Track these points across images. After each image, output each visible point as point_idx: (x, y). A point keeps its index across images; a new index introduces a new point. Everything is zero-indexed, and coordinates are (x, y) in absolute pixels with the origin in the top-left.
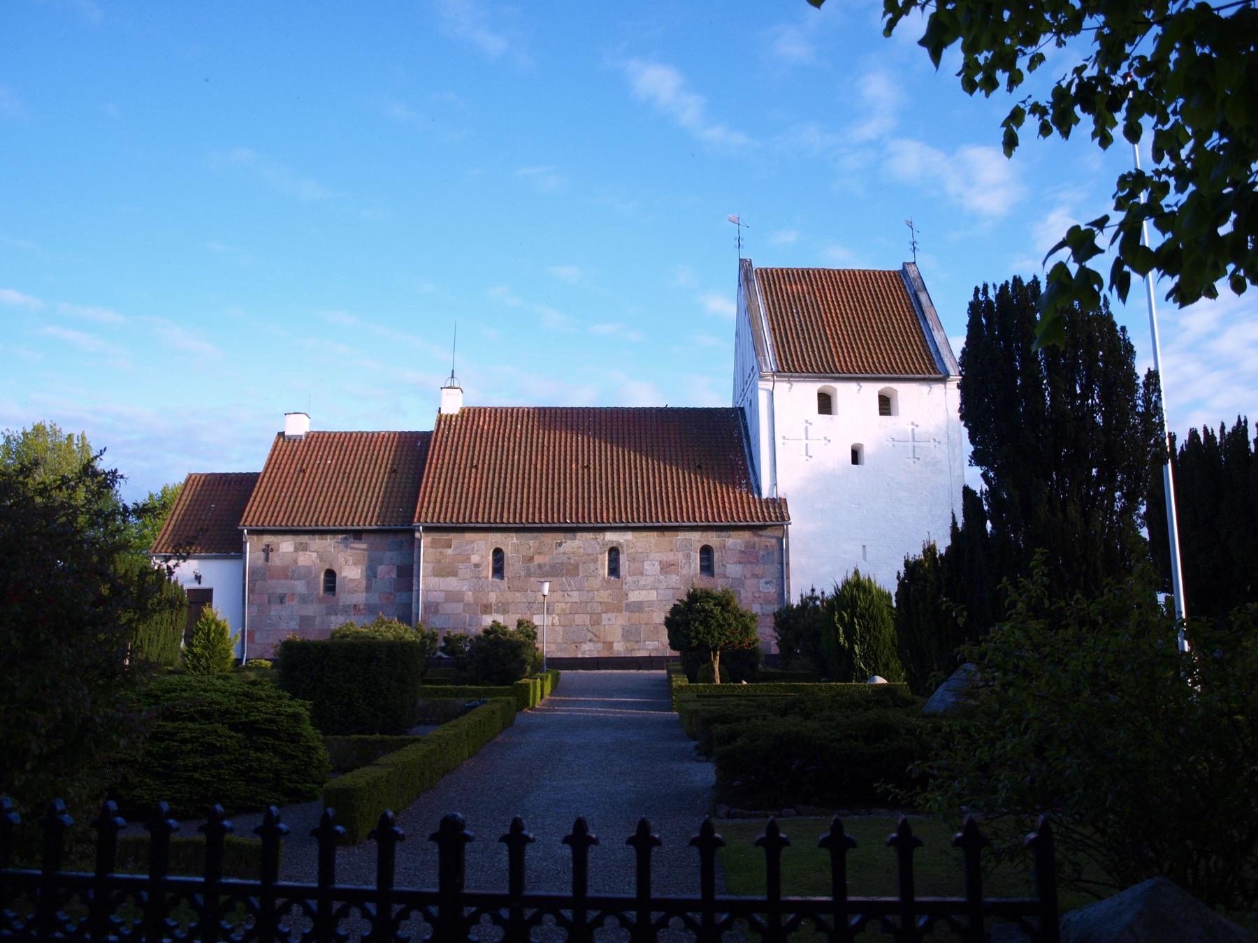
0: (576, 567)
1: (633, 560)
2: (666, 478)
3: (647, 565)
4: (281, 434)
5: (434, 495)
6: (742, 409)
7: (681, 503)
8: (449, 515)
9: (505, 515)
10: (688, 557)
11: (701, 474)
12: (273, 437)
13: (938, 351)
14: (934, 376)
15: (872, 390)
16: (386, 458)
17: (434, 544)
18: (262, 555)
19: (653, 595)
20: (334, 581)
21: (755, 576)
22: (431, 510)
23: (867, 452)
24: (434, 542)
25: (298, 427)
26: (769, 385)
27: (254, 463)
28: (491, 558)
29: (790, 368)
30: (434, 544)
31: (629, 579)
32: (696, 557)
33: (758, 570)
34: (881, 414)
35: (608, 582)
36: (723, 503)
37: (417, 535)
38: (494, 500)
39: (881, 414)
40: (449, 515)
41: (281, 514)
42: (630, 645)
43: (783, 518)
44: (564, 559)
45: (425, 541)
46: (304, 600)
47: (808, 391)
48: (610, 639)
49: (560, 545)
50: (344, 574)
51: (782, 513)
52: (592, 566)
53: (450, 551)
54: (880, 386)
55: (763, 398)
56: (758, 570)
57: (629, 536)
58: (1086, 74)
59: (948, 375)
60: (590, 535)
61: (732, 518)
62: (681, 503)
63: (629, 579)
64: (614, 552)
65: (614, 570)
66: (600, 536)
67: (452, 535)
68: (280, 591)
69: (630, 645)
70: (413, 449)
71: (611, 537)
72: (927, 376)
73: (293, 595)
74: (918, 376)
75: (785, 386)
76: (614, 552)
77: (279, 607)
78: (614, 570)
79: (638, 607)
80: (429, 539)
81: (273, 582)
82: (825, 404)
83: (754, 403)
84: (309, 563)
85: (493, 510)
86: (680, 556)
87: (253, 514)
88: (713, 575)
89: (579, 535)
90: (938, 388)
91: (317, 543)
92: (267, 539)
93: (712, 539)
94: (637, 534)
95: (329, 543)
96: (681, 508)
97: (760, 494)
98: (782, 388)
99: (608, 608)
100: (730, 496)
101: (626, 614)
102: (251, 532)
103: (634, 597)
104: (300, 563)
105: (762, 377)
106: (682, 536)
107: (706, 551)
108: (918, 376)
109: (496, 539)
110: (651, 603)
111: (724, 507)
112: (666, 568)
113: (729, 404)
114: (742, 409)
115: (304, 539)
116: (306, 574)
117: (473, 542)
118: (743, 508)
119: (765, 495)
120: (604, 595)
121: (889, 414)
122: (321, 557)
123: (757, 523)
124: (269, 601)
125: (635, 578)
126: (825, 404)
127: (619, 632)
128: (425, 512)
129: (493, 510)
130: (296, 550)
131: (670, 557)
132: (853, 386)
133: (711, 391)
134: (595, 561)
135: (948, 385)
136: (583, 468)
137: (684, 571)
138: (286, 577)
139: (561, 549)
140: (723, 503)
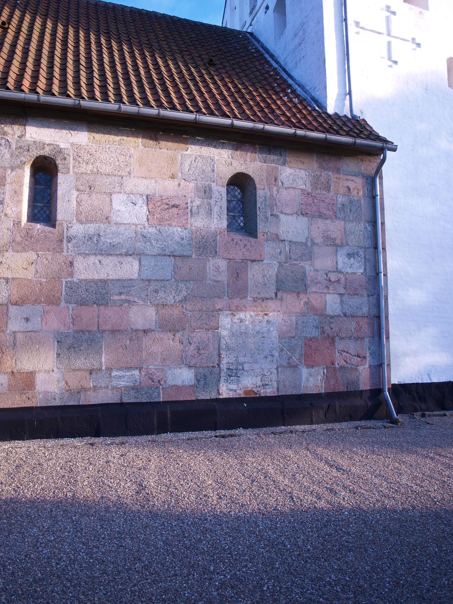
64: (45, 171)
76: (45, 171)
88: (256, 237)
110: (125, 285)
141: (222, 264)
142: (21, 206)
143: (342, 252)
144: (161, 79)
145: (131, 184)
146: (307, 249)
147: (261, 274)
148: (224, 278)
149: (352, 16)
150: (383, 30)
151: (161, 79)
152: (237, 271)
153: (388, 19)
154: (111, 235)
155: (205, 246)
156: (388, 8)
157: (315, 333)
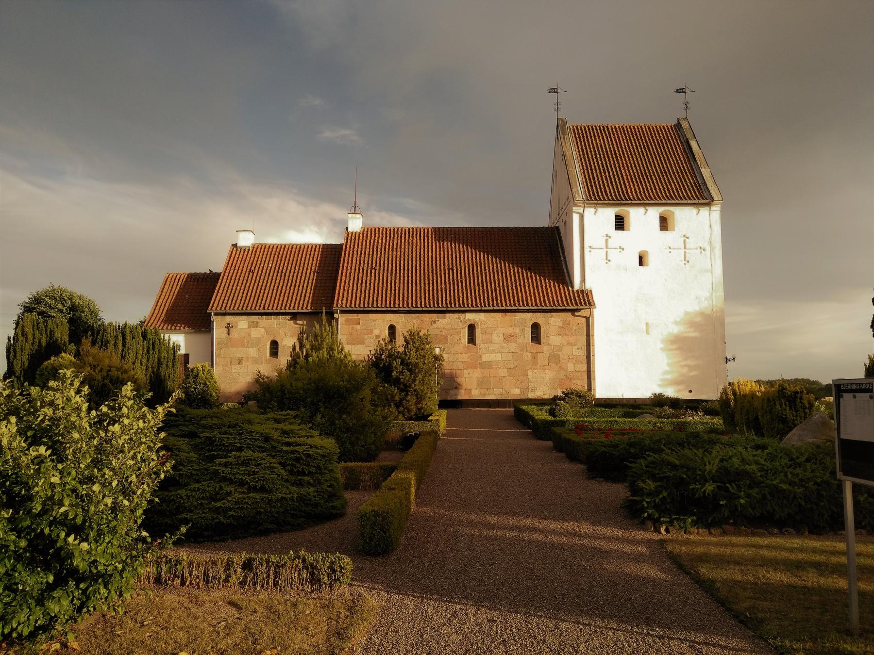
0: (446, 338)
1: (485, 333)
2: (506, 277)
3: (494, 336)
4: (235, 245)
5: (346, 288)
6: (558, 228)
7: (517, 294)
8: (358, 302)
9: (397, 302)
10: (523, 330)
11: (544, 277)
12: (228, 249)
13: (705, 183)
14: (702, 201)
15: (654, 214)
16: (314, 263)
17: (348, 322)
18: (226, 330)
19: (498, 357)
20: (277, 348)
21: (570, 344)
22: (345, 299)
23: (651, 259)
24: (347, 320)
25: (246, 240)
26: (581, 210)
27: (218, 265)
28: (387, 332)
29: (598, 195)
30: (348, 322)
31: (482, 346)
32: (528, 330)
33: (572, 339)
34: (661, 230)
35: (468, 348)
36: (547, 293)
37: (336, 316)
38: (389, 292)
39: (661, 230)
40: (358, 302)
41: (238, 302)
42: (483, 391)
43: (590, 304)
44: (438, 332)
45: (342, 318)
46: (256, 361)
47: (608, 214)
48: (469, 387)
49: (435, 322)
50: (284, 343)
51: (589, 300)
52: (457, 337)
53: (359, 327)
54: (661, 209)
55: (576, 218)
56: (572, 339)
57: (482, 316)
58: (39, 622)
59: (713, 200)
60: (456, 315)
61: (554, 304)
62: (517, 294)
63: (482, 346)
64: (472, 328)
65: (472, 339)
66: (462, 316)
67: (360, 316)
68: (238, 355)
69: (483, 391)
70: (330, 257)
71: (470, 317)
72: (697, 201)
73: (248, 358)
74: (690, 201)
75: (592, 210)
76: (472, 328)
77: (238, 367)
78: (472, 339)
79: (488, 365)
80: (344, 319)
81: (233, 350)
82: (620, 223)
83: (568, 224)
84: (259, 336)
85: (388, 299)
86: (517, 330)
87: (217, 302)
88: (540, 344)
89: (448, 315)
90: (704, 211)
91: (264, 321)
92: (228, 319)
93: (539, 318)
94: (486, 314)
95: (273, 321)
96: (518, 297)
97: (572, 287)
98: (589, 212)
99: (469, 366)
100: (551, 287)
101: (480, 370)
102: (216, 314)
103: (486, 358)
104: (252, 336)
105: (576, 205)
106: (519, 315)
107: (536, 328)
108: (690, 201)
109: (391, 318)
110: (497, 362)
111: (548, 297)
112: (508, 338)
113: (546, 224)
114: (558, 228)
115: (255, 318)
116: (257, 343)
117: (374, 321)
118: (561, 297)
119: (577, 286)
120: (465, 357)
121: (667, 230)
122: (267, 332)
123: (571, 307)
124: (231, 363)
125: (486, 345)
126: (620, 223)
127: (476, 383)
128: (341, 300)
129: (388, 299)
130: (250, 327)
131: (510, 331)
132: (641, 210)
133: (538, 218)
134: (459, 333)
135: (713, 208)
136: (449, 269)
137: (520, 341)
138: (243, 345)
139: (435, 326)
140: (547, 293)
141: (529, 354)
142: (465, 340)
143: (575, 348)
144: (604, 186)
145: (498, 330)
146: (560, 348)
147: (542, 359)
148: (529, 359)
149: (587, 244)
150: (604, 246)
151: (604, 186)
152: (534, 358)
153: (607, 241)
154: (402, 386)
155: (523, 348)
156: (607, 235)
157: (563, 377)
